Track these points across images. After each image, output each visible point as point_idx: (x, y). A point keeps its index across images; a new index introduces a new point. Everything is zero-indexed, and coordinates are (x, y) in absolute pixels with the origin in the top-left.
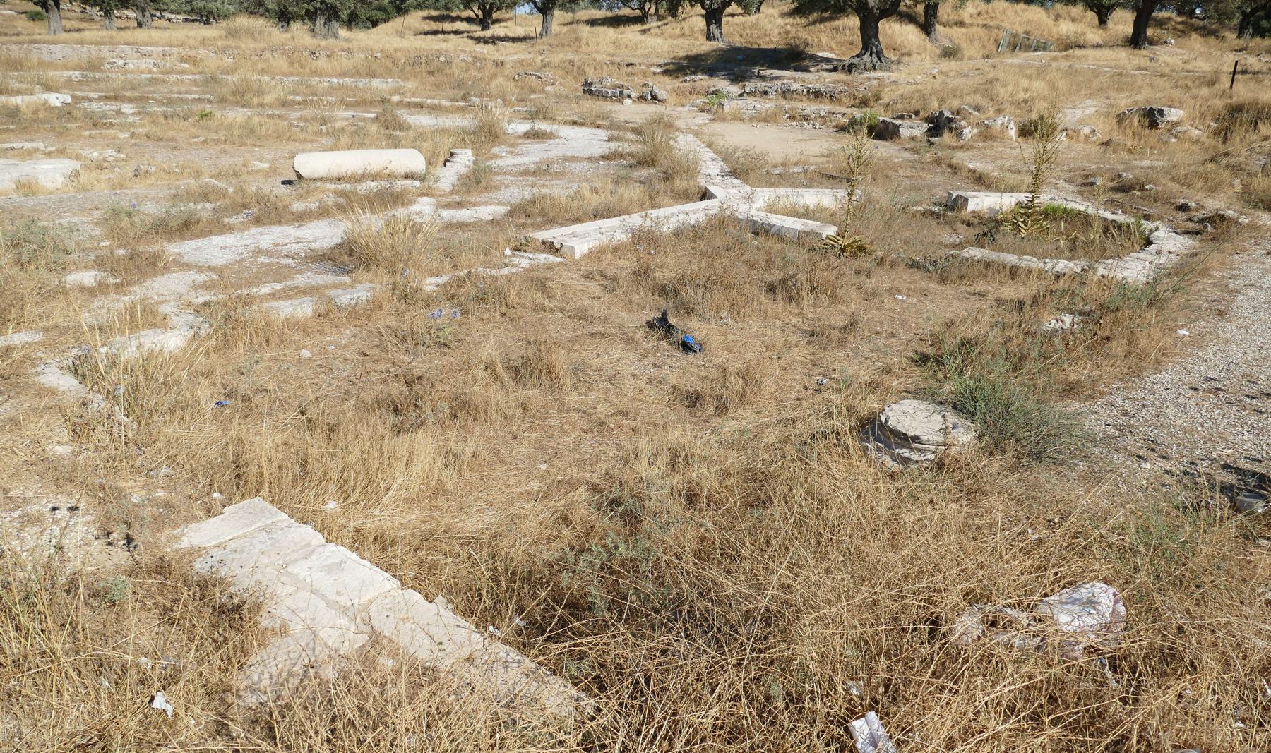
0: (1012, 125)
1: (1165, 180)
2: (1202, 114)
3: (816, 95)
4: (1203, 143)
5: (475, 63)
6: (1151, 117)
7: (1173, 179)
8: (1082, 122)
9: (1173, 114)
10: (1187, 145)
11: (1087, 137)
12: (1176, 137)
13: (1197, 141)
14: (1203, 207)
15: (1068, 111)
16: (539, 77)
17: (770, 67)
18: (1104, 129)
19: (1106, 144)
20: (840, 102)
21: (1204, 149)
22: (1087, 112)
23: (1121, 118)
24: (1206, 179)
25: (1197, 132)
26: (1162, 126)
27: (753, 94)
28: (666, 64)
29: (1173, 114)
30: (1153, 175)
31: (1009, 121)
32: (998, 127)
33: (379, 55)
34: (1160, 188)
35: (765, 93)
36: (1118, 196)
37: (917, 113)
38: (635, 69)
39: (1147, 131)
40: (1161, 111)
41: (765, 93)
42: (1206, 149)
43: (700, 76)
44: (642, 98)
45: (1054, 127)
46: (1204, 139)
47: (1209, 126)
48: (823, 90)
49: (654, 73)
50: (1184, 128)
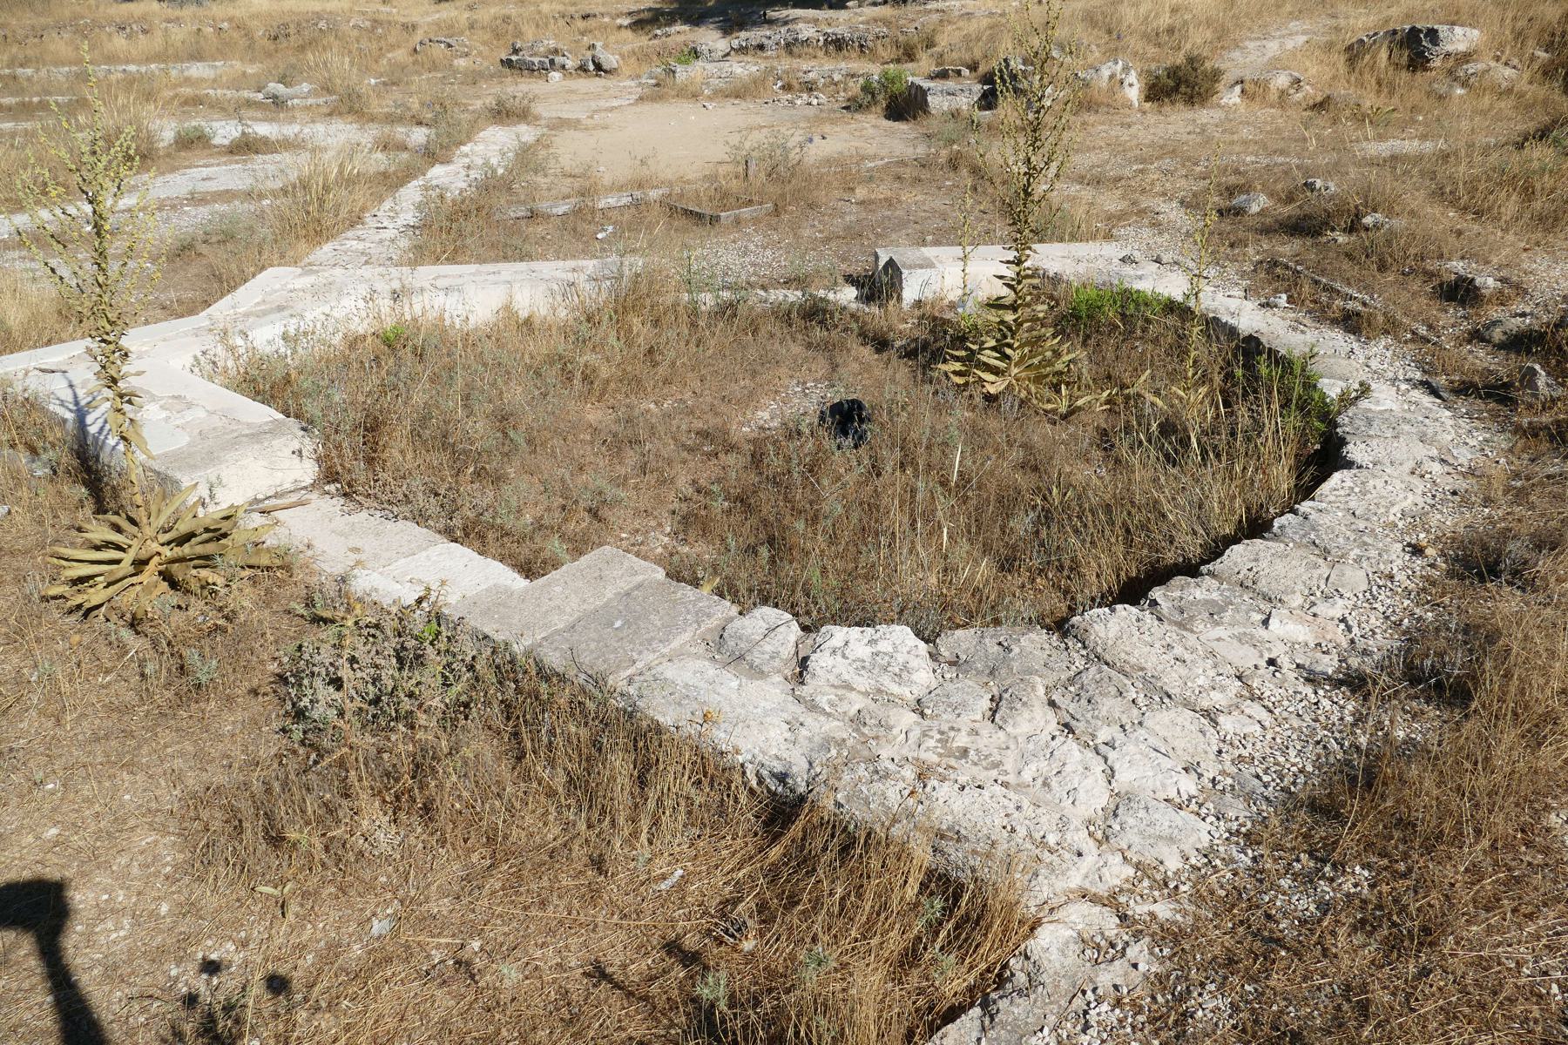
0: (1132, 77)
1: (1416, 198)
2: (1519, 35)
3: (837, 45)
4: (1521, 95)
5: (374, 28)
6: (1414, 46)
7: (1439, 194)
8: (1275, 65)
9: (1459, 39)
10: (1486, 100)
11: (1283, 93)
12: (1465, 84)
13: (1509, 91)
14: (1520, 290)
15: (1251, 45)
16: (449, 46)
17: (795, 6)
18: (1319, 75)
19: (1320, 106)
20: (874, 57)
21: (1525, 106)
22: (1290, 44)
23: (1354, 53)
24: (1528, 193)
25: (1508, 72)
26: (1437, 63)
27: (742, 50)
28: (639, 12)
29: (1459, 39)
30: (1387, 184)
31: (1126, 69)
32: (1104, 84)
33: (225, 25)
34: (1399, 223)
35: (761, 47)
36: (1287, 248)
37: (973, 67)
38: (591, 23)
39: (1405, 75)
40: (1433, 34)
41: (761, 47)
42: (1529, 107)
43: (678, 27)
44: (582, 68)
45: (1216, 75)
46: (1523, 85)
47: (1533, 58)
48: (847, 36)
49: (620, 27)
50: (1481, 66)
